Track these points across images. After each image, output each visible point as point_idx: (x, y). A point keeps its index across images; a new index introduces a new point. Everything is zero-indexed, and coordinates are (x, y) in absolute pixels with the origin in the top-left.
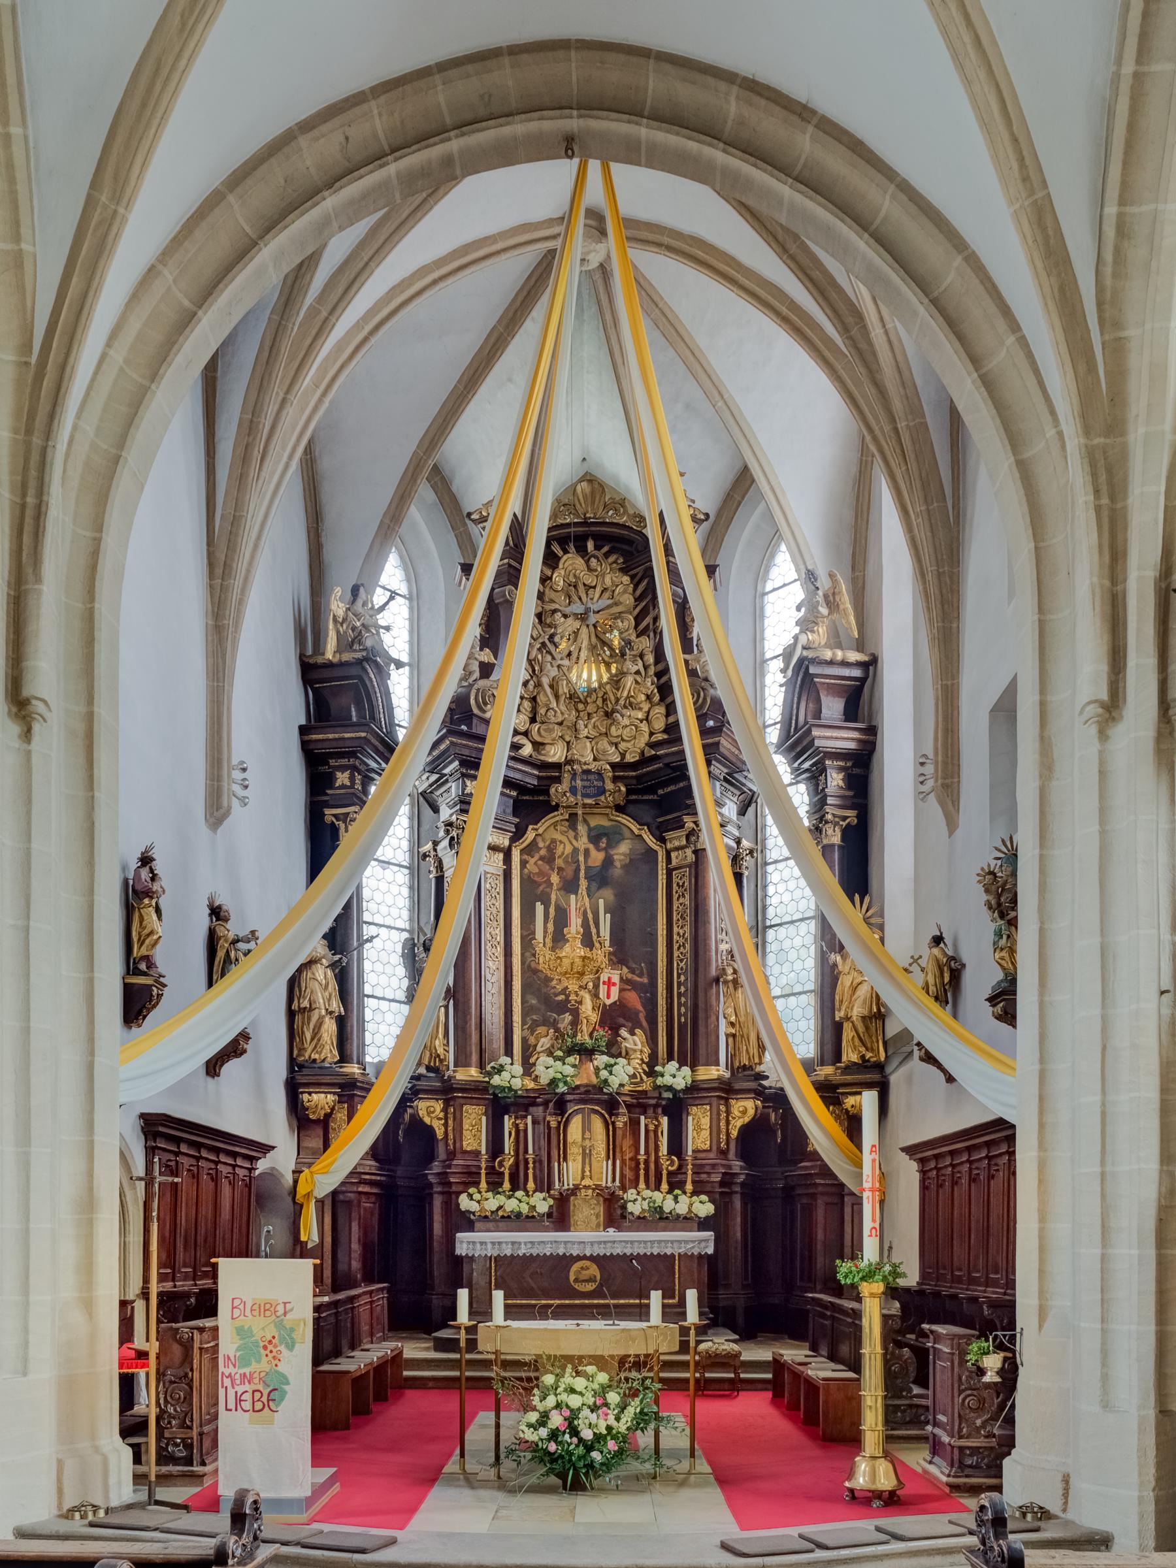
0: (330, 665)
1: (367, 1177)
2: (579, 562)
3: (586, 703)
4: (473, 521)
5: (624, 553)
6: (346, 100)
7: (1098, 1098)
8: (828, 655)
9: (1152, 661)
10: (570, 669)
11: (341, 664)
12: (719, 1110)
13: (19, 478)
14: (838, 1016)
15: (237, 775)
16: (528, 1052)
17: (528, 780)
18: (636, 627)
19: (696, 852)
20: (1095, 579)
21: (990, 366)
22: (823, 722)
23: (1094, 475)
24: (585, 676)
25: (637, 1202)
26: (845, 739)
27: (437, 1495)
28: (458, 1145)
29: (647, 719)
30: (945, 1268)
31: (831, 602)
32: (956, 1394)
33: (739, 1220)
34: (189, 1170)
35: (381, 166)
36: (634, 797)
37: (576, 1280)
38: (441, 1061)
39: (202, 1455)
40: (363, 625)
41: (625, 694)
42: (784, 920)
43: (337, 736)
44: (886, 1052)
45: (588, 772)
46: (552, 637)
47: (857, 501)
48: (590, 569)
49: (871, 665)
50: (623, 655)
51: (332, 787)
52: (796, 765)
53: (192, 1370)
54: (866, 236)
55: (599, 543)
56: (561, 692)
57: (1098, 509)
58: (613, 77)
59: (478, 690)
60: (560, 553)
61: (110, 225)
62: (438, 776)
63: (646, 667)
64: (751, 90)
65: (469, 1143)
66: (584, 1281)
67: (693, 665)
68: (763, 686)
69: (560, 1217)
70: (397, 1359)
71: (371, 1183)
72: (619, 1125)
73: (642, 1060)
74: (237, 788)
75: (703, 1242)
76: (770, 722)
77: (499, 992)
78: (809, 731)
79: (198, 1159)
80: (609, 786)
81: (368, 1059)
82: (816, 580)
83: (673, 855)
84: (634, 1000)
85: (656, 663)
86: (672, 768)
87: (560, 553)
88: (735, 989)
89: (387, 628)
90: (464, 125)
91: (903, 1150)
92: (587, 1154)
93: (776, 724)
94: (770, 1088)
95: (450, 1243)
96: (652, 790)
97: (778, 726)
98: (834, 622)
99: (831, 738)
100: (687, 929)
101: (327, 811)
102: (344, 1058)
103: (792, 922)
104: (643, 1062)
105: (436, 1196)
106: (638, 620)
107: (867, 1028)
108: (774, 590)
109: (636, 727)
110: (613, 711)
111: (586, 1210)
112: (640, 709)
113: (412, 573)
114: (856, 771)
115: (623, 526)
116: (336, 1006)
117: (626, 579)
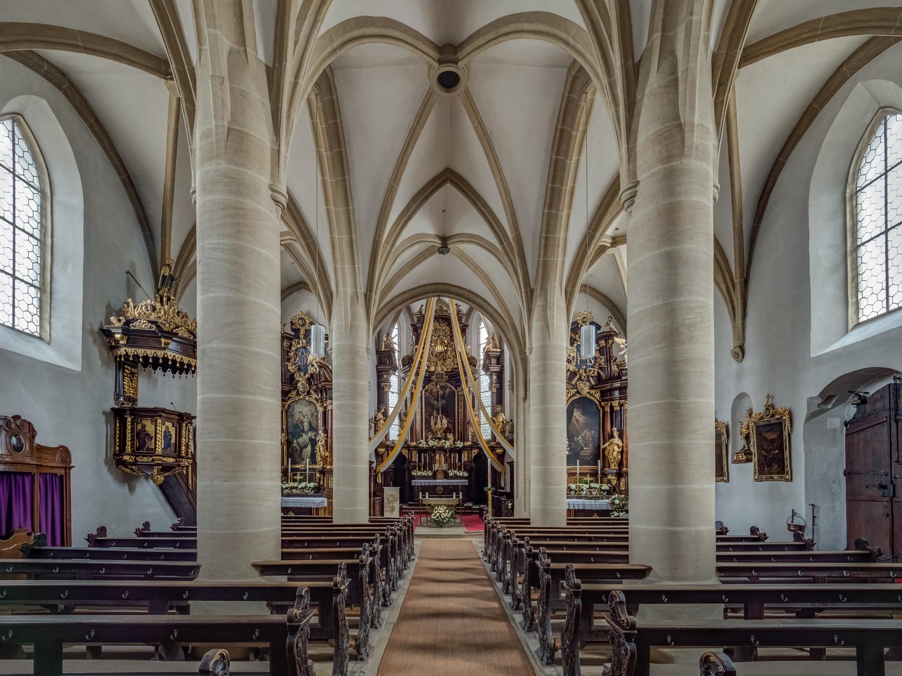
16: (426, 438)
25: (451, 473)
26: (496, 369)
31: (493, 338)
49: (502, 352)
58: (447, 288)
69: (434, 477)
75: (465, 482)
84: (450, 426)
92: (441, 463)
95: (410, 483)
111: (439, 475)
113: (399, 329)
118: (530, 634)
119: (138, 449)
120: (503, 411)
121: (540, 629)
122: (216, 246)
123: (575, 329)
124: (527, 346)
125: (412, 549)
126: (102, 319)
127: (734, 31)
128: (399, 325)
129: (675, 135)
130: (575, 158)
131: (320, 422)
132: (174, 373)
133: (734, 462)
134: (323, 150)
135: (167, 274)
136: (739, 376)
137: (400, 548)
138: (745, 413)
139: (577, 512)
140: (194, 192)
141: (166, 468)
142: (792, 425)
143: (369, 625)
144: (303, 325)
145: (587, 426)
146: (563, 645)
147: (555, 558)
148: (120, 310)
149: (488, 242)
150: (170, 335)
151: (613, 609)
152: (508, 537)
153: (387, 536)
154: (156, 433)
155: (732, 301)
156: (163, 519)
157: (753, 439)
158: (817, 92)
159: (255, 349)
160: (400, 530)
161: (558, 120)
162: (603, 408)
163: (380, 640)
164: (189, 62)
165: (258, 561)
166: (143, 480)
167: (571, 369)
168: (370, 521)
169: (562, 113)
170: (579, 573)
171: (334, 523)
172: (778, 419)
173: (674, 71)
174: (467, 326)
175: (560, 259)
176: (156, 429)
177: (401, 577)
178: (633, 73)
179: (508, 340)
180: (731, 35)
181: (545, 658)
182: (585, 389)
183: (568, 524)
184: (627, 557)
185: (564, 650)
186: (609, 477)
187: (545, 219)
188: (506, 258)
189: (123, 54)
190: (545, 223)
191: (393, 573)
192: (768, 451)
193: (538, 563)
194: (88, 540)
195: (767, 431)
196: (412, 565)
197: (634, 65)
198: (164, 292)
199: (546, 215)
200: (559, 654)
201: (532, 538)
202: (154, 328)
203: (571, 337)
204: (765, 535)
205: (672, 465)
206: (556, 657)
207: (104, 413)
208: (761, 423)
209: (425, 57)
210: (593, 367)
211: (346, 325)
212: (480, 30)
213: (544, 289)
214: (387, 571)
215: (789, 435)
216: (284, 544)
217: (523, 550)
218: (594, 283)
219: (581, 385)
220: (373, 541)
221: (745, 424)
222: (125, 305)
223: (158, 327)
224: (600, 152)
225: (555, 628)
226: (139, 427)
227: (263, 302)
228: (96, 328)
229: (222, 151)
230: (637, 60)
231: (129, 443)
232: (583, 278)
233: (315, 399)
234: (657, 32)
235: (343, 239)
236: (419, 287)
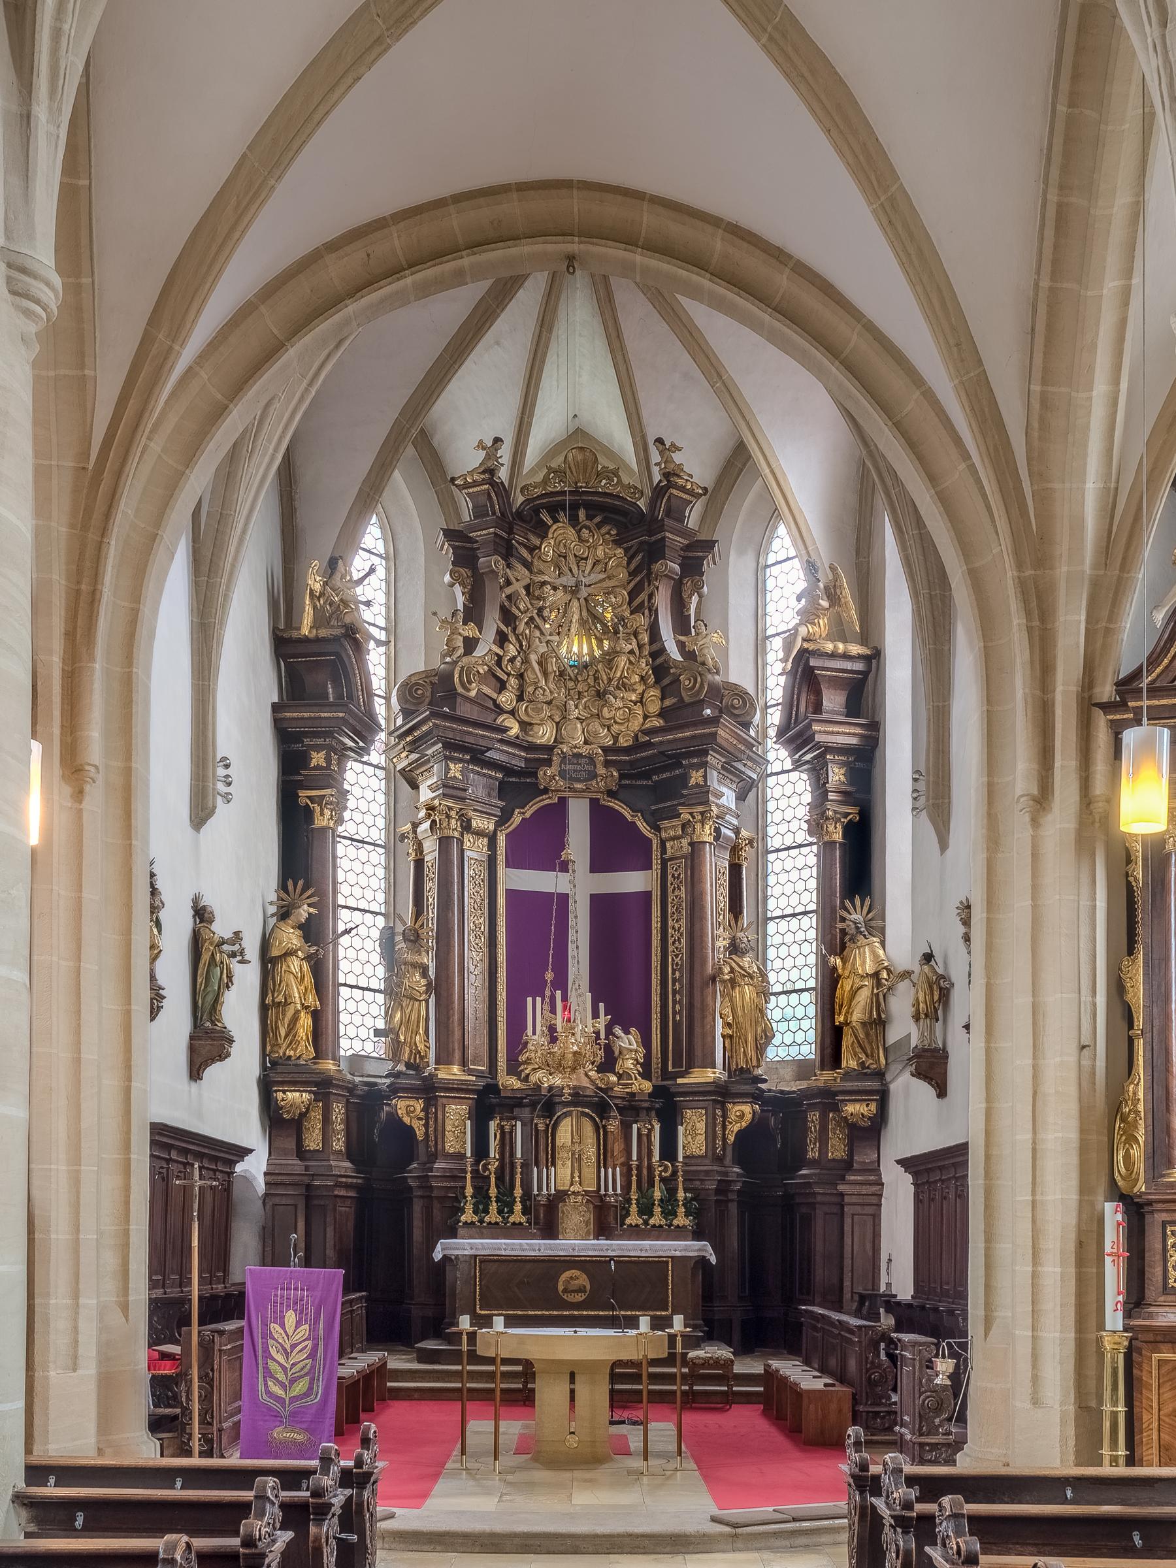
0: (306, 640)
1: (344, 1180)
2: (571, 532)
3: (576, 681)
4: (457, 486)
5: (616, 524)
6: (369, 225)
7: (1029, 1136)
8: (829, 647)
9: (1073, 764)
10: (559, 644)
11: (318, 640)
12: (714, 1114)
13: (74, 567)
14: (840, 1019)
15: (221, 772)
17: (514, 762)
18: (630, 603)
19: (691, 844)
20: (1027, 690)
21: (946, 484)
22: (825, 716)
23: (1026, 602)
24: (575, 649)
26: (847, 735)
27: (440, 1486)
28: (440, 1147)
29: (641, 702)
30: (935, 1282)
31: (832, 594)
32: (917, 1396)
33: (735, 1229)
34: (160, 1173)
35: (399, 279)
36: (627, 782)
37: (565, 1291)
38: (421, 1058)
39: (221, 1450)
40: (341, 600)
41: (618, 675)
42: (786, 912)
43: (312, 715)
44: (886, 1059)
45: (579, 755)
46: (540, 610)
47: (862, 484)
48: (581, 540)
49: (874, 658)
50: (616, 632)
51: (307, 768)
52: (797, 756)
53: (212, 1370)
54: (837, 363)
55: (591, 512)
56: (550, 669)
57: (1030, 629)
58: (612, 211)
59: (462, 668)
60: (550, 522)
61: (165, 359)
62: (418, 756)
63: (640, 647)
64: (733, 233)
65: (451, 1146)
66: (573, 1291)
67: (690, 646)
68: (765, 664)
70: (380, 1372)
71: (348, 1186)
72: (610, 1128)
73: (637, 1060)
74: (221, 787)
76: (773, 702)
77: (483, 985)
78: (809, 726)
79: (168, 1161)
80: (601, 770)
81: (342, 1053)
82: (817, 571)
83: (668, 845)
85: (651, 642)
86: (667, 756)
87: (550, 522)
88: (733, 988)
89: (368, 604)
90: (475, 245)
91: (898, 1162)
92: (574, 1161)
93: (777, 705)
94: (770, 1090)
96: (647, 775)
97: (780, 707)
98: (838, 613)
99: (833, 733)
100: (683, 922)
101: (302, 793)
102: (319, 1055)
103: (794, 915)
104: (638, 1063)
105: (415, 1200)
106: (633, 595)
107: (867, 1035)
108: (777, 563)
109: (630, 709)
110: (605, 692)
111: (575, 1216)
112: (634, 690)
113: (391, 534)
114: (858, 765)
115: (618, 497)
116: (312, 999)
117: (619, 552)
120: (876, 928)
174: (709, 545)
193: (879, 1503)
236: (458, 198)
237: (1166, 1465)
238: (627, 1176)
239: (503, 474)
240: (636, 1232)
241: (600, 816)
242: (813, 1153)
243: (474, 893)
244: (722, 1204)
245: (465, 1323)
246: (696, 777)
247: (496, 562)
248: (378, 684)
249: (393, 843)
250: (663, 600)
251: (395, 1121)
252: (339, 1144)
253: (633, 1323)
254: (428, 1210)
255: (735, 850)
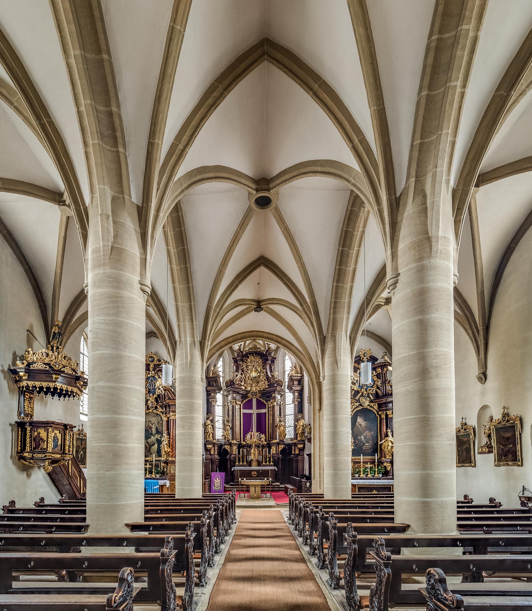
26: (298, 388)
31: (295, 367)
58: (260, 334)
92: (254, 455)
111: (254, 463)
118: (323, 571)
119: (34, 449)
120: (303, 418)
121: (329, 566)
122: (103, 321)
123: (358, 360)
124: (321, 375)
125: (235, 516)
126: (9, 361)
127: (467, 175)
128: (224, 358)
129: (425, 243)
130: (356, 249)
131: (165, 428)
132: (60, 397)
133: (479, 453)
134: (171, 248)
135: (57, 331)
136: (483, 393)
137: (226, 515)
138: (487, 419)
139: (362, 488)
140: (87, 286)
141: (54, 462)
142: (522, 427)
143: (207, 564)
144: (153, 361)
145: (368, 428)
146: (345, 575)
147: (341, 520)
148: (22, 356)
149: (291, 304)
150: (59, 372)
151: (377, 549)
152: (307, 507)
153: (218, 506)
154: (48, 438)
155: (477, 342)
156: (52, 498)
157: (494, 437)
158: (522, 222)
159: (129, 386)
160: (227, 502)
161: (343, 225)
162: (380, 415)
163: (213, 574)
164: (84, 204)
165: (129, 522)
166: (36, 469)
167: (355, 389)
168: (203, 496)
169: (346, 220)
170: (356, 529)
171: (176, 498)
172: (511, 423)
173: (425, 203)
175: (345, 316)
176: (48, 435)
177: (227, 534)
178: (396, 204)
179: (307, 369)
180: (466, 177)
181: (333, 585)
182: (366, 403)
183: (352, 497)
184: (393, 519)
185: (345, 578)
186: (385, 464)
187: (334, 290)
188: (305, 315)
189: (30, 191)
190: (334, 292)
191: (222, 532)
192: (505, 446)
193: (328, 523)
194: (3, 510)
195: (504, 432)
196: (234, 526)
197: (396, 198)
198: (54, 343)
199: (334, 287)
200: (342, 582)
201: (324, 507)
202: (48, 368)
203: (355, 367)
204: (500, 503)
205: (424, 458)
206: (340, 584)
207: (10, 425)
208: (499, 426)
209: (246, 187)
210: (372, 387)
211: (187, 363)
212: (286, 170)
213: (334, 337)
214: (218, 530)
215: (520, 434)
216: (146, 512)
217: (318, 515)
218: (372, 329)
219: (363, 400)
220: (208, 510)
221: (487, 427)
222: (27, 353)
223: (51, 367)
224: (372, 249)
225: (340, 566)
226: (36, 434)
227: (135, 356)
228: (6, 369)
229: (107, 261)
230: (398, 194)
231: (28, 445)
232: (365, 325)
233: (161, 412)
234: (412, 177)
235: (183, 305)
236: (239, 334)
237: (266, 470)
238: (263, 457)
239: (242, 349)
240: (264, 466)
241: (258, 401)
242: (293, 453)
243: (237, 413)
244: (278, 461)
245: (240, 479)
246: (273, 395)
247: (241, 363)
248: (222, 382)
249: (224, 406)
250: (268, 367)
251: (225, 449)
252: (216, 453)
253: (264, 479)
254: (230, 463)
255: (280, 405)
